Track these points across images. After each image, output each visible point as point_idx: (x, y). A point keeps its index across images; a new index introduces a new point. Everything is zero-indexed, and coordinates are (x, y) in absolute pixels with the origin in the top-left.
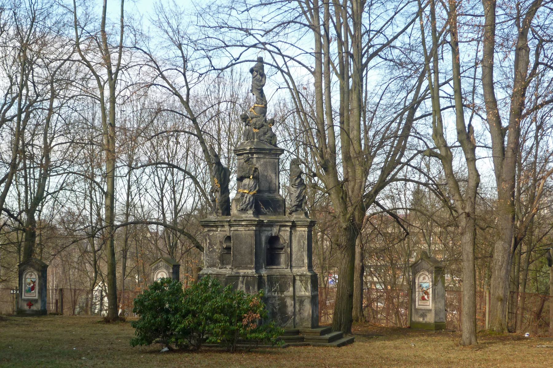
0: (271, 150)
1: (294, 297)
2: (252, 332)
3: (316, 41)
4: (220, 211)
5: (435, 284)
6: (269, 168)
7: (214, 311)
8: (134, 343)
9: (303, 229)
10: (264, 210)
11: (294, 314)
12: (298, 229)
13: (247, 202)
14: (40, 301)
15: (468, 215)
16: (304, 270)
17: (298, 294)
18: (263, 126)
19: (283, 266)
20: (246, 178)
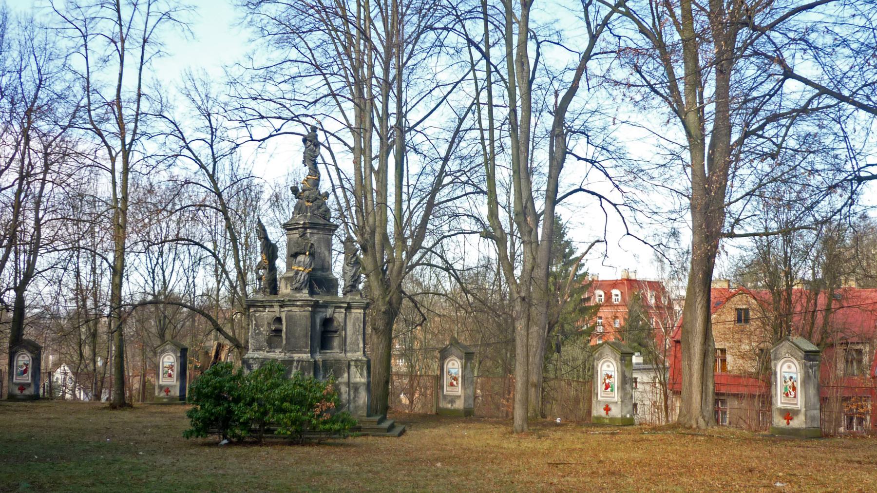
0: (325, 225)
1: (348, 384)
2: (325, 423)
3: (356, 116)
4: (268, 290)
5: (464, 368)
6: (322, 244)
7: (283, 400)
8: (189, 434)
9: (359, 311)
10: (317, 290)
11: (349, 402)
12: (353, 311)
13: (302, 280)
14: (33, 385)
15: (523, 299)
16: (359, 355)
17: (353, 380)
18: (316, 199)
19: (337, 350)
20: (301, 254)
